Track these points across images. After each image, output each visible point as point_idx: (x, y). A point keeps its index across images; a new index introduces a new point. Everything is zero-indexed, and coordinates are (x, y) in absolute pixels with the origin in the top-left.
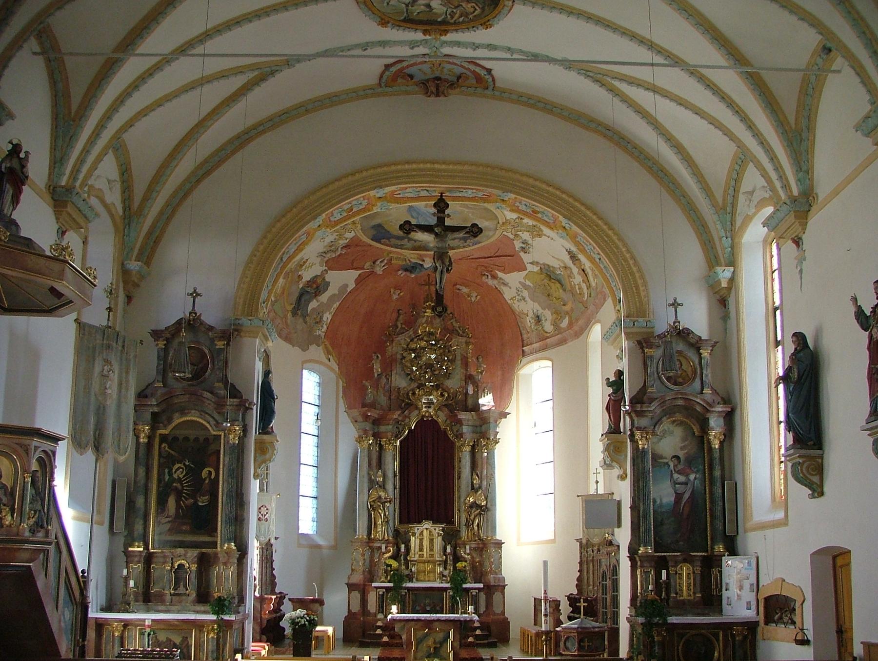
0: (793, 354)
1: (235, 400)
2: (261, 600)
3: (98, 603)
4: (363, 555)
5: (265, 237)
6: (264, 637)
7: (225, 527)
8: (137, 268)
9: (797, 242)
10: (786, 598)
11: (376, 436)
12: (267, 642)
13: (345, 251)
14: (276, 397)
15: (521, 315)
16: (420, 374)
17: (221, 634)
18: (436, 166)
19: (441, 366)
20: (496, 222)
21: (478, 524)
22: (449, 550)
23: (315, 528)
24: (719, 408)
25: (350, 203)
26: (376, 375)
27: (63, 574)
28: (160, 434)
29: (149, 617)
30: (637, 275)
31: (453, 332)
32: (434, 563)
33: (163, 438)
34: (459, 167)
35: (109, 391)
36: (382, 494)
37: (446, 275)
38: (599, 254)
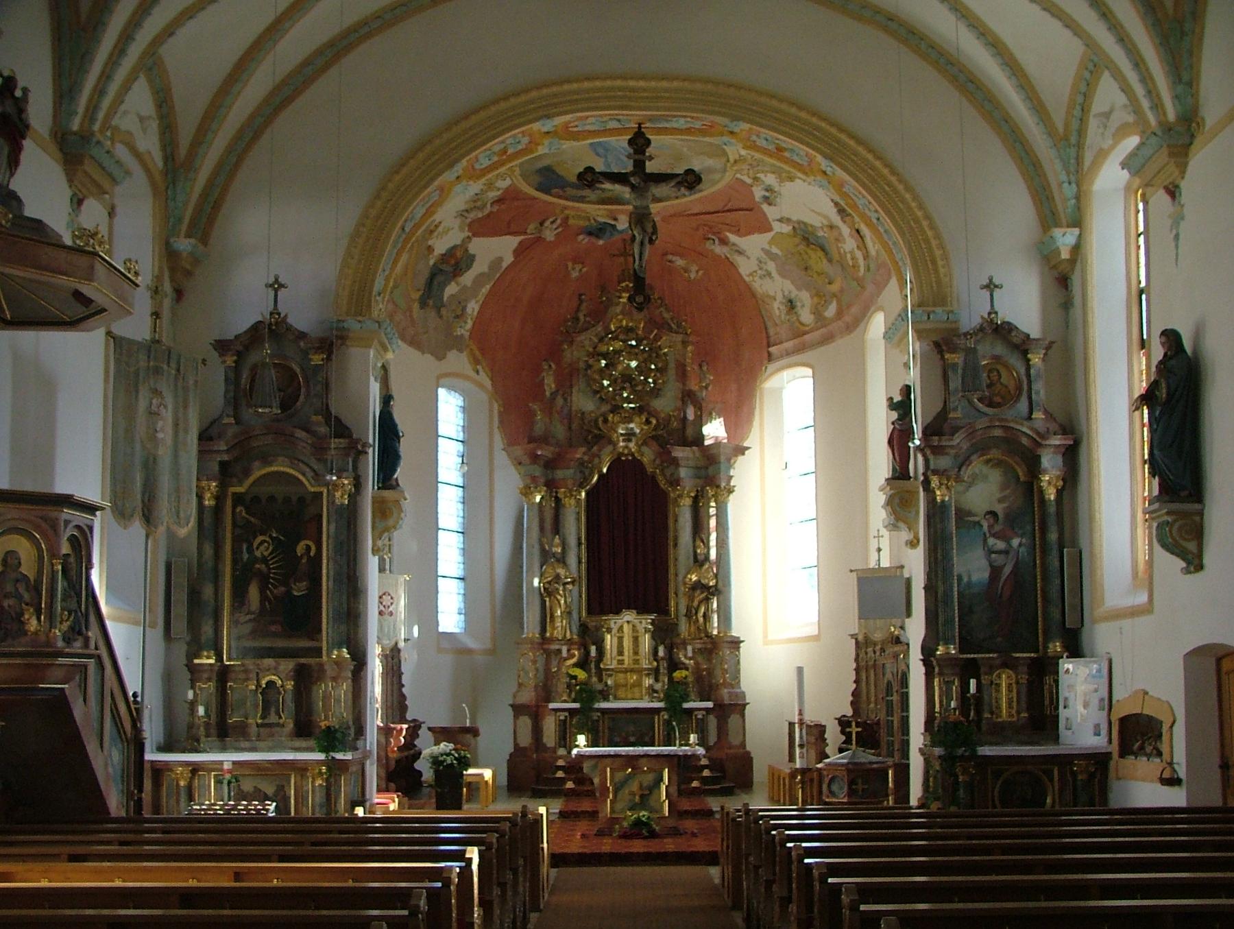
0: (1160, 362)
1: (342, 440)
2: (386, 731)
3: (154, 739)
4: (534, 662)
5: (378, 197)
6: (392, 785)
7: (333, 627)
8: (189, 248)
9: (1173, 192)
10: (1150, 719)
11: (551, 485)
12: (397, 791)
13: (497, 207)
14: (401, 434)
15: (766, 299)
16: (614, 390)
17: (332, 780)
18: (632, 83)
19: (646, 379)
20: (724, 160)
21: (704, 613)
22: (661, 653)
23: (462, 625)
24: (1056, 441)
25: (503, 142)
26: (548, 394)
27: (108, 700)
28: (234, 494)
29: (228, 758)
30: (934, 243)
31: (663, 326)
32: (639, 671)
33: (238, 499)
34: (665, 84)
35: (160, 435)
36: (561, 571)
37: (647, 247)
38: (876, 211)
